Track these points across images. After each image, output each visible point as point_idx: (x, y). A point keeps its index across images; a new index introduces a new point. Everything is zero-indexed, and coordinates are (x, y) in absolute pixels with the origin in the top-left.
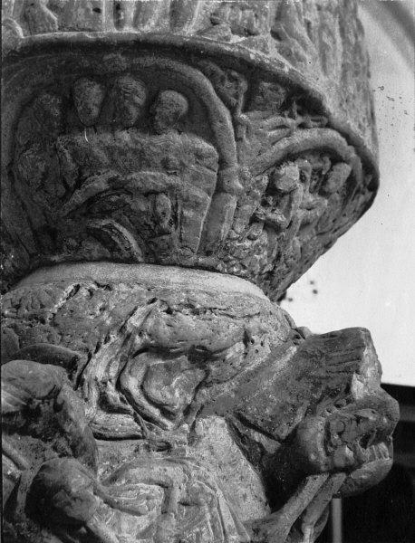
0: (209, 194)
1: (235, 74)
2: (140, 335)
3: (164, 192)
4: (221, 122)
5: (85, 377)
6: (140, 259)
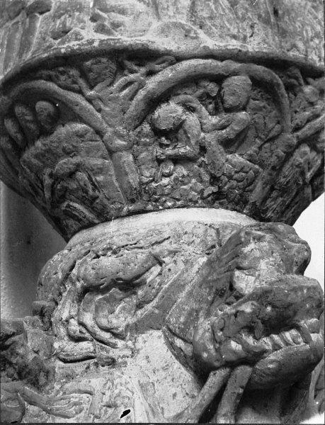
0: (105, 158)
1: (61, 69)
2: (79, 281)
3: (77, 170)
4: (77, 105)
5: (52, 320)
6: (96, 221)
